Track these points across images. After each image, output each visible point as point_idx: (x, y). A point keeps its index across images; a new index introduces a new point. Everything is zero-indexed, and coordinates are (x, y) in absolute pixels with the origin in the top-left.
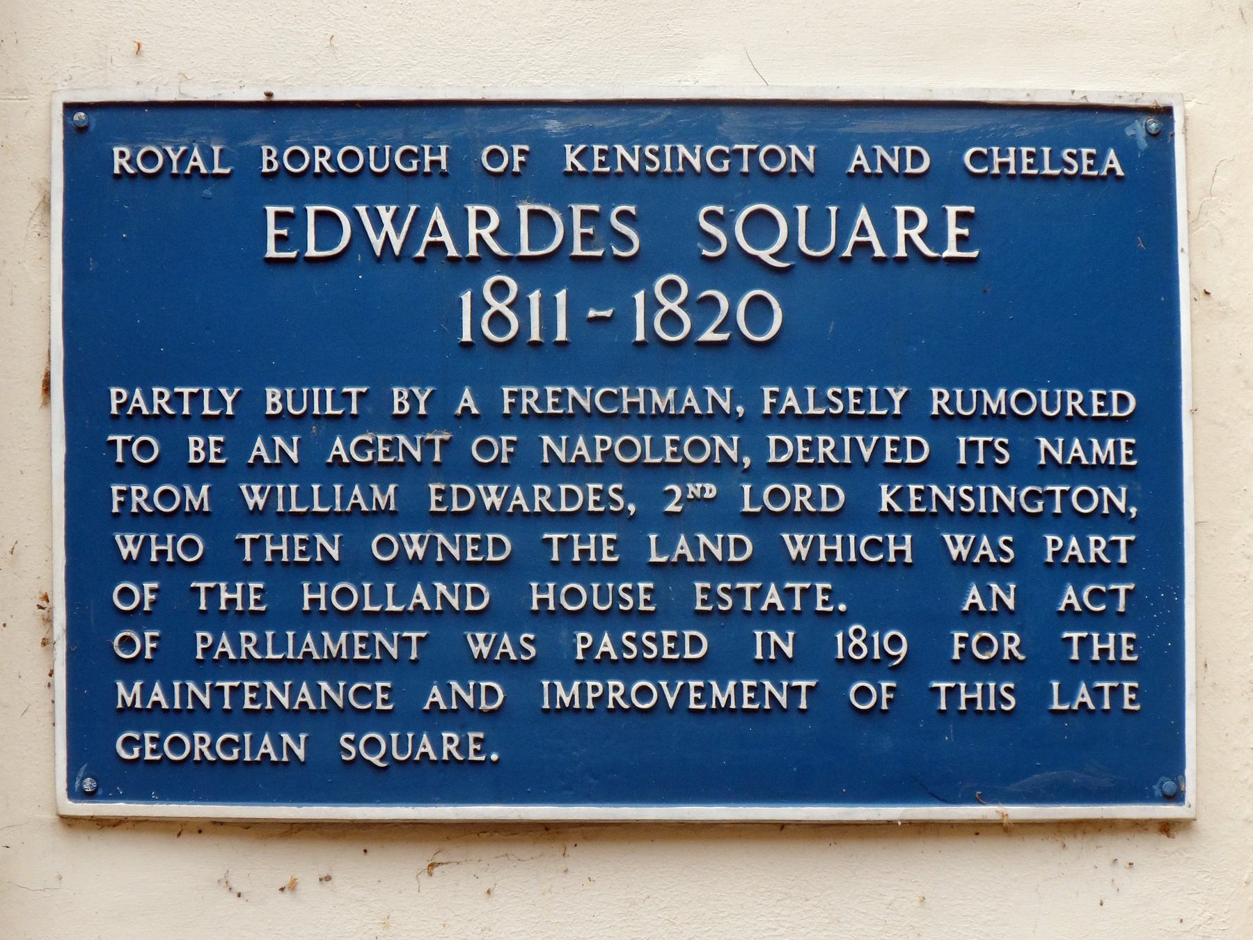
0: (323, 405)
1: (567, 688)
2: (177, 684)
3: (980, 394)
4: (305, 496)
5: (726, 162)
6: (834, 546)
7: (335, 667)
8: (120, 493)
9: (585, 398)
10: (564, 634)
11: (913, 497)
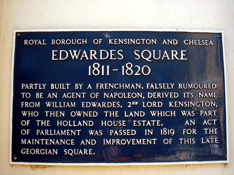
0: (62, 87)
1: (108, 141)
2: (33, 140)
3: (188, 85)
4: (58, 105)
5: (140, 42)
6: (160, 114)
7: (64, 137)
8: (23, 103)
9: (113, 86)
10: (108, 130)
11: (175, 104)
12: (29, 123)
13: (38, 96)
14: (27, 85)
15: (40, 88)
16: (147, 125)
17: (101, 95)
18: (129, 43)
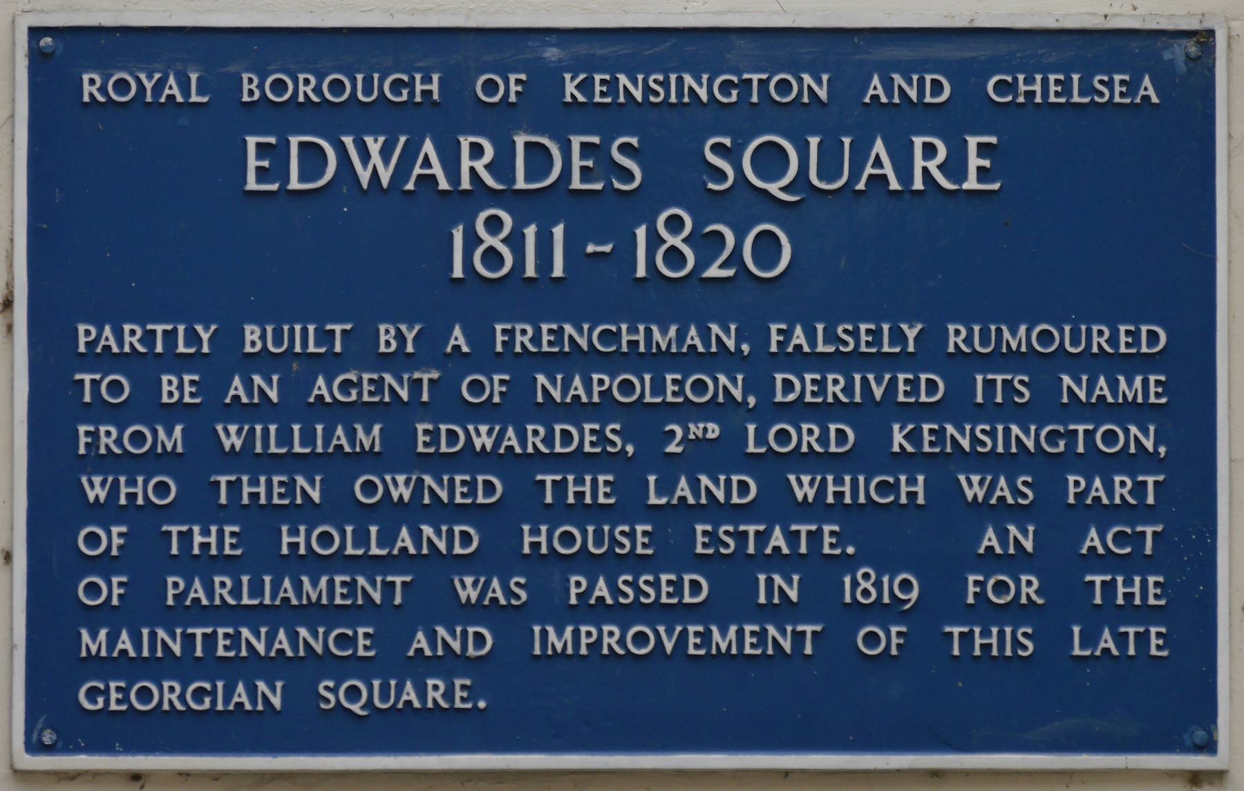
1: (560, 633)
2: (145, 632)
3: (999, 331)
4: (285, 437)
7: (316, 614)
11: (927, 437)
12: (122, 541)
13: (171, 394)
14: (107, 330)
15: (181, 349)
16: (768, 551)
17: (520, 389)
18: (673, 99)
